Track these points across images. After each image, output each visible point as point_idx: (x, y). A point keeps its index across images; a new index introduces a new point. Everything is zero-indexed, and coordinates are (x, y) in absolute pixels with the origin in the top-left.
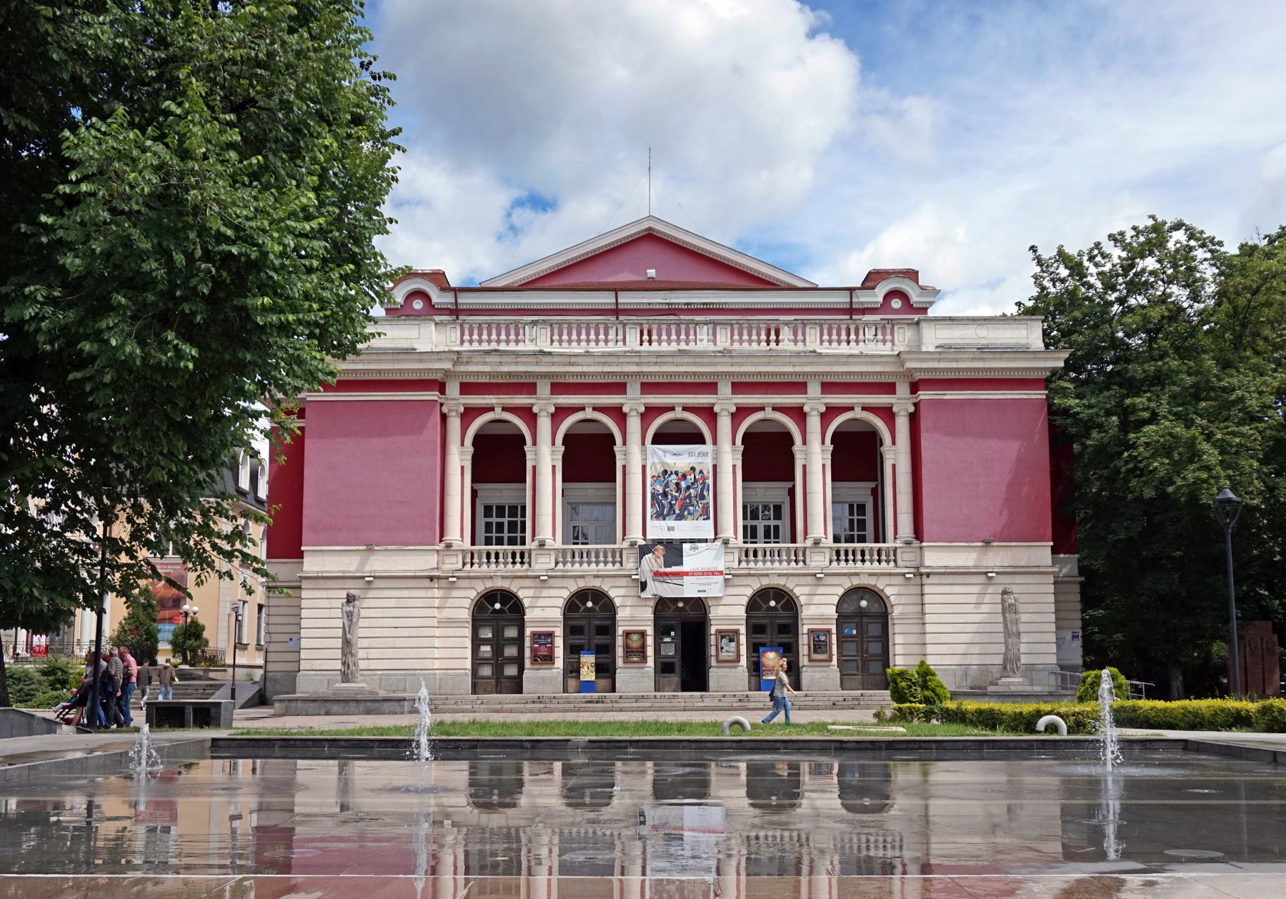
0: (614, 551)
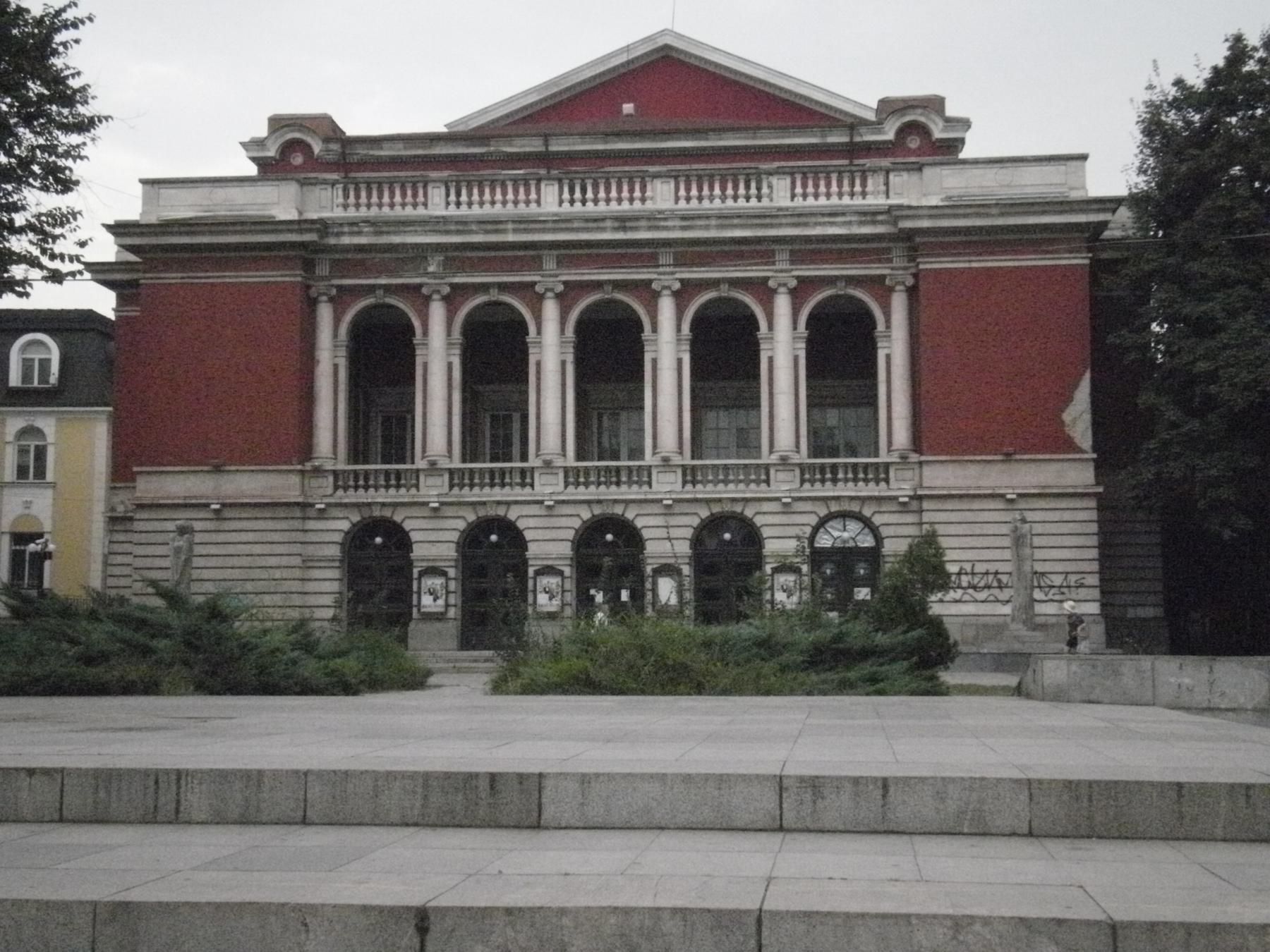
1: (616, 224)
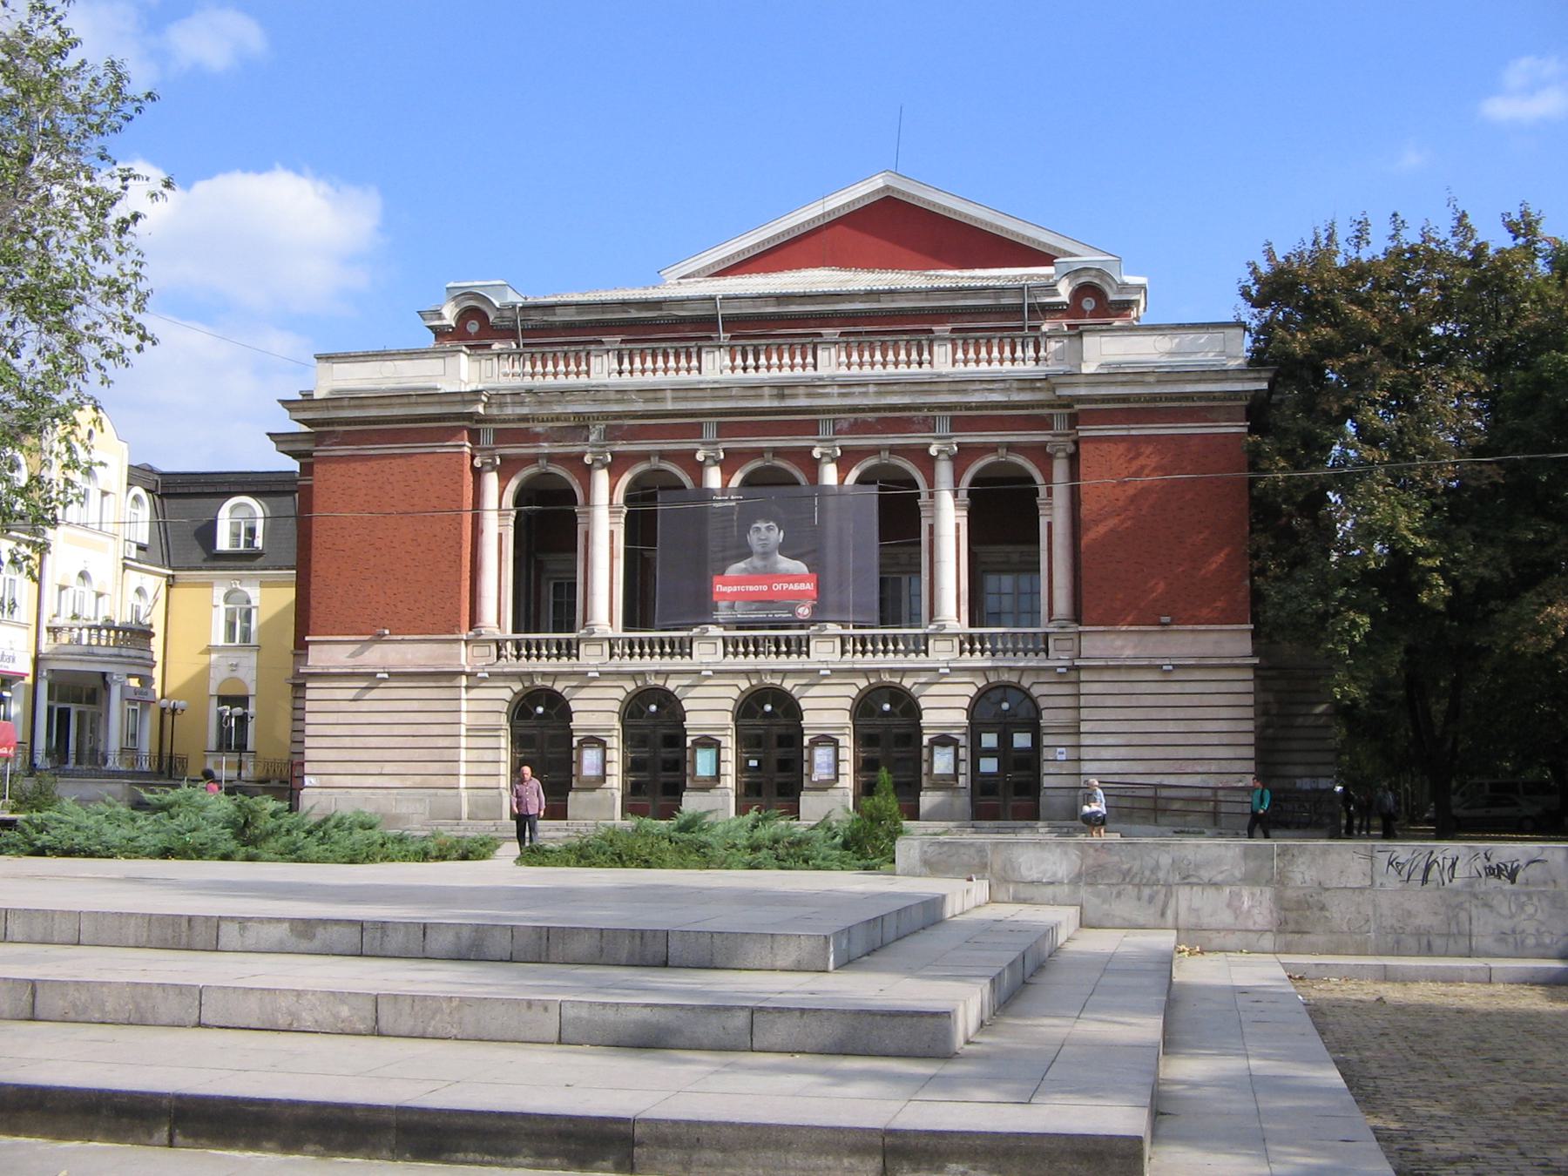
0: (569, 642)
1: (775, 392)
